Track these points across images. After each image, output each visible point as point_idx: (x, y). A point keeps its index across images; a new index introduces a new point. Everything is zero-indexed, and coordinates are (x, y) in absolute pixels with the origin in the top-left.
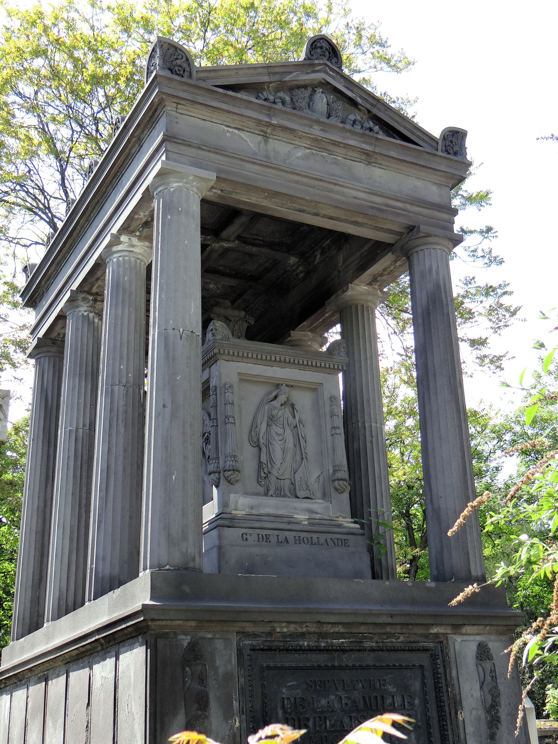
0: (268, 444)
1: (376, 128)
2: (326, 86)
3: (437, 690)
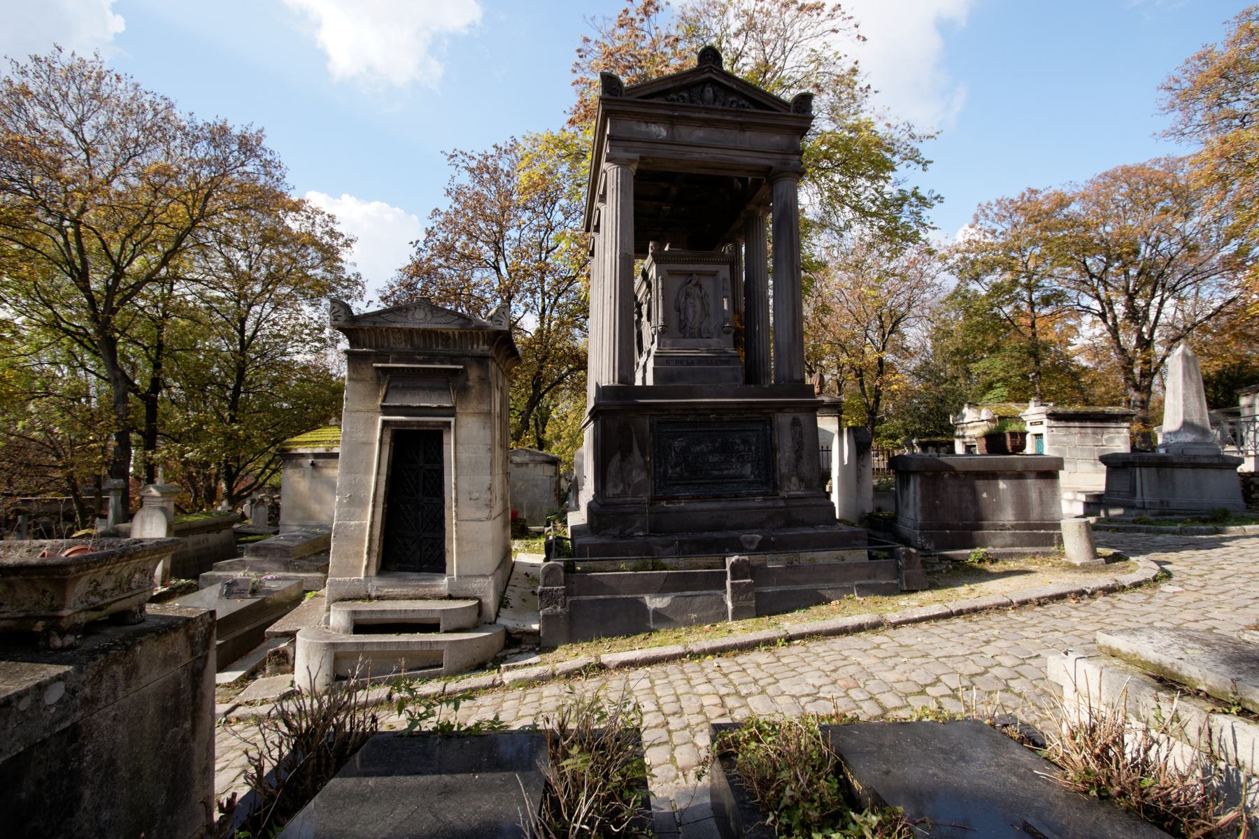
0: (686, 309)
1: (747, 104)
2: (711, 82)
3: (129, 643)
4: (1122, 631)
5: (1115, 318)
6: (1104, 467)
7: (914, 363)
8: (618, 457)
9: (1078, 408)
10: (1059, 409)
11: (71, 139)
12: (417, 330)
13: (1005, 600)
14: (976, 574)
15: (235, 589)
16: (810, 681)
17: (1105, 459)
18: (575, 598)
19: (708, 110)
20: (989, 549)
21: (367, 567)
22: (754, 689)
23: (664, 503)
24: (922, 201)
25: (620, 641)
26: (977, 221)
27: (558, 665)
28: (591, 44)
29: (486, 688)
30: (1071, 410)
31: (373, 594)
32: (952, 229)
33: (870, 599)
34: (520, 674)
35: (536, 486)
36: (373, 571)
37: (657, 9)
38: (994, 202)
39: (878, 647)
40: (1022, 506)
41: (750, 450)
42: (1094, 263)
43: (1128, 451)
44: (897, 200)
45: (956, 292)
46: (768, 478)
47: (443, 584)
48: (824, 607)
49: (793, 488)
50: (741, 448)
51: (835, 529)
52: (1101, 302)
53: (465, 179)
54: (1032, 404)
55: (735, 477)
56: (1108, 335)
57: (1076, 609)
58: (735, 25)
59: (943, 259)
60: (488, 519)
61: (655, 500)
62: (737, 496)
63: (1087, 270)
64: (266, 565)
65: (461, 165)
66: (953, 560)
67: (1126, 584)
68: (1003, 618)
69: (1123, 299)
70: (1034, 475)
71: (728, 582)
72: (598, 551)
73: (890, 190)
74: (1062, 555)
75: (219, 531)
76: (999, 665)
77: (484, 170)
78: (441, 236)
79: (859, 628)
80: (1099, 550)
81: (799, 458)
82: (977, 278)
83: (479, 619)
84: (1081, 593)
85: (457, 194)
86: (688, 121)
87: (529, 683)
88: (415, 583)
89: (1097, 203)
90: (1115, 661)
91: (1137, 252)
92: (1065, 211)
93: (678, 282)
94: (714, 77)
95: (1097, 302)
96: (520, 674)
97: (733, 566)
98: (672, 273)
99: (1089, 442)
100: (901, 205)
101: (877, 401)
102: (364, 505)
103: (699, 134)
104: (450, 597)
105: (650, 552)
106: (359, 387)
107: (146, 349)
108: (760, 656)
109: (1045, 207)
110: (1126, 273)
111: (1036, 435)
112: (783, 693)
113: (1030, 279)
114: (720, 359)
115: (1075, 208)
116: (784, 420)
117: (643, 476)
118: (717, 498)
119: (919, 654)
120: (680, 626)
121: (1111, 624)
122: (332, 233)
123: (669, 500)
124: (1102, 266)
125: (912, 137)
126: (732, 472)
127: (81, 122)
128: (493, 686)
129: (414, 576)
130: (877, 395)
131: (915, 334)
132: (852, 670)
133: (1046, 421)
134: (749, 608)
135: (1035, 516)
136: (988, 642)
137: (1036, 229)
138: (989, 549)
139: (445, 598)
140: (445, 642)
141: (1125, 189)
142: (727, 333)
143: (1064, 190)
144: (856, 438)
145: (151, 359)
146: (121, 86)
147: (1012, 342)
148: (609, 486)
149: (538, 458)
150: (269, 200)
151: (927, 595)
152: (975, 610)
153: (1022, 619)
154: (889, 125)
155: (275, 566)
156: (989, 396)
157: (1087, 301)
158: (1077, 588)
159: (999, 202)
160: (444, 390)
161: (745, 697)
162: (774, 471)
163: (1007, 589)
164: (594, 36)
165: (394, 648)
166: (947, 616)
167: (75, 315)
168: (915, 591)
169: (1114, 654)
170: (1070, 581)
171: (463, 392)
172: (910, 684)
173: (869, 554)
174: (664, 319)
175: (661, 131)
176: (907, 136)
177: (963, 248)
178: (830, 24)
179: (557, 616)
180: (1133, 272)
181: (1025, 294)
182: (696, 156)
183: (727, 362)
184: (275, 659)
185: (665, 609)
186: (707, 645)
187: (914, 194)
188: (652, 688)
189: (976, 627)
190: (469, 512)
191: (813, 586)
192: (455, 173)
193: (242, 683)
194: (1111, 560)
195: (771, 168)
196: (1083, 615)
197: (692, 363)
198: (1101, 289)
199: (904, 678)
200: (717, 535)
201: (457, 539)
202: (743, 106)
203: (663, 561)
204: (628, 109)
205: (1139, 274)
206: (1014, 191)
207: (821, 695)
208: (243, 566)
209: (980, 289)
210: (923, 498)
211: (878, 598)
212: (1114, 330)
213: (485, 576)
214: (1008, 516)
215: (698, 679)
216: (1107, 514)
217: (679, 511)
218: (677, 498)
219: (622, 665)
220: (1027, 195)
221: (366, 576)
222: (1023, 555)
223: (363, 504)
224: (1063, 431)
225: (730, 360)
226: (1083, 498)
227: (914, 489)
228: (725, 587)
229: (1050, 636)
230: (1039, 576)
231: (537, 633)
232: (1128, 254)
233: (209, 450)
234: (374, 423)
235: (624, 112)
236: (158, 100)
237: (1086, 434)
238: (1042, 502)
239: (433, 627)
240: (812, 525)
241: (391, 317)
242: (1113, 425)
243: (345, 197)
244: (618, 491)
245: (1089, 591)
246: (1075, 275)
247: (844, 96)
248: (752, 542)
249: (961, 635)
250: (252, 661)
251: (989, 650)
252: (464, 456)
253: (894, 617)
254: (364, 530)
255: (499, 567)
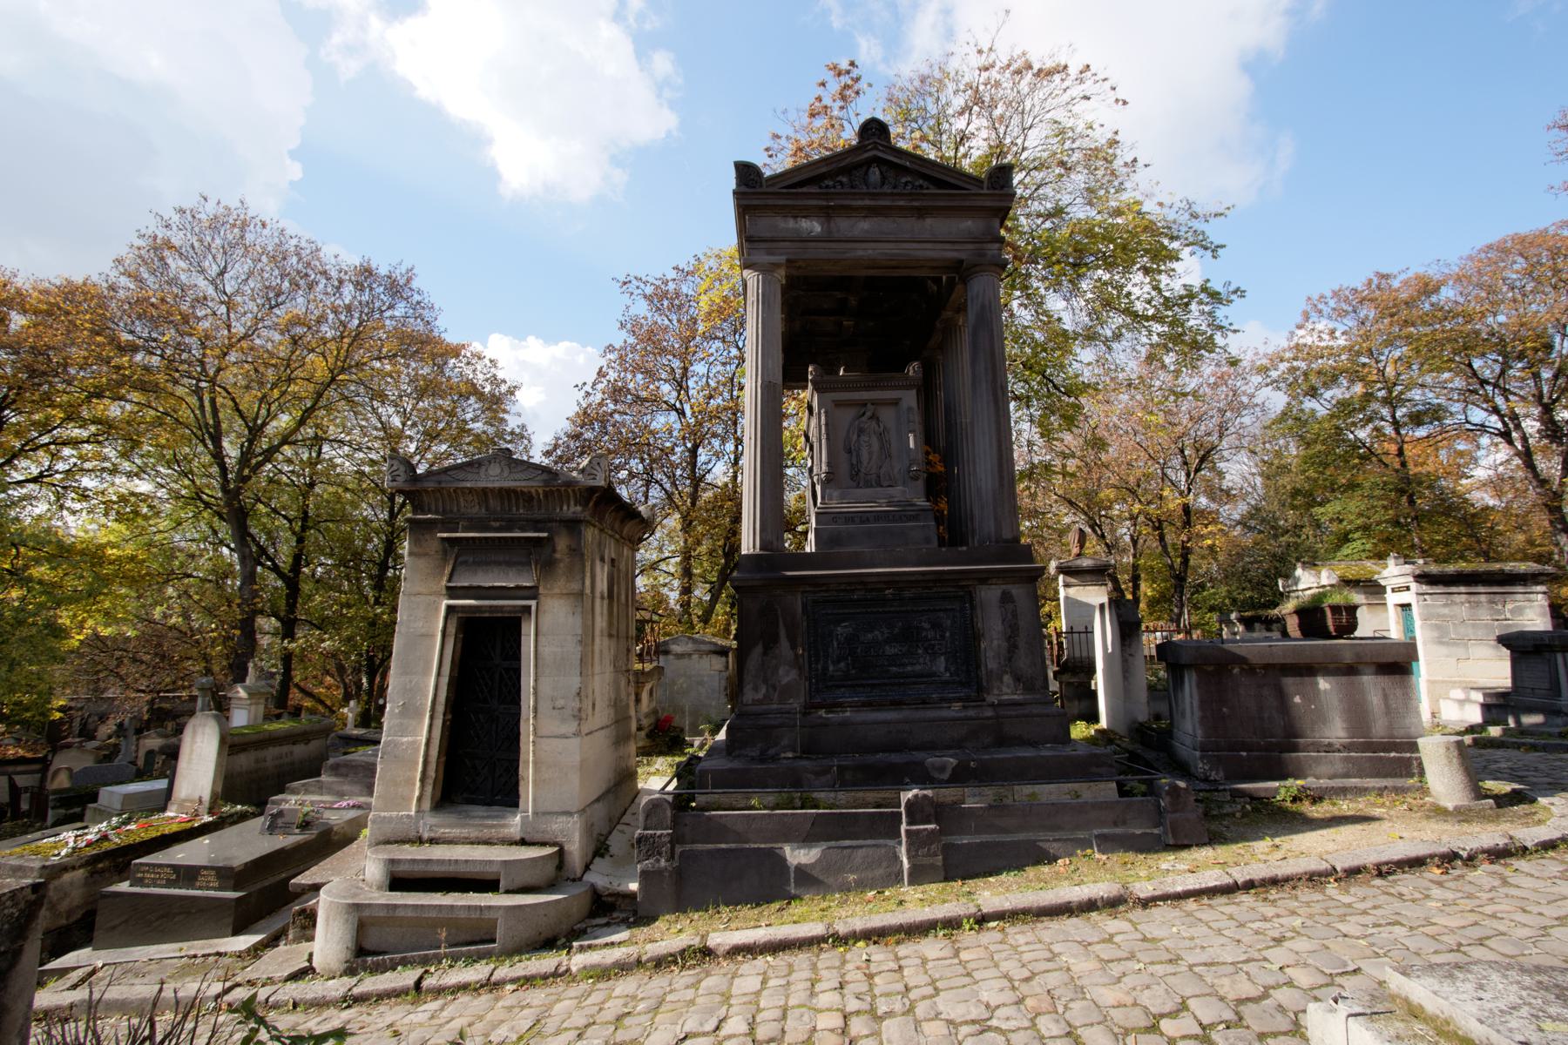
1: (925, 184)
4: (1432, 967)
5: (1524, 439)
6: (1506, 652)
7: (1238, 510)
8: (759, 649)
9: (1481, 566)
10: (1434, 569)
11: (211, 291)
12: (492, 490)
13: (1324, 866)
14: (1287, 820)
15: (280, 821)
16: (985, 996)
17: (1505, 640)
18: (688, 847)
19: (873, 196)
20: (1310, 781)
21: (420, 799)
22: (898, 1007)
23: (822, 713)
24: (1215, 296)
25: (746, 912)
26: (1307, 318)
27: (649, 947)
28: (783, 142)
29: (545, 977)
30: (1451, 568)
31: (426, 836)
32: (1257, 334)
33: (1117, 858)
34: (593, 958)
35: (701, 683)
36: (427, 805)
37: (857, 93)
38: (1329, 294)
39: (1110, 939)
40: (1357, 716)
41: (943, 637)
42: (1486, 366)
43: (1550, 628)
44: (1181, 298)
45: (1284, 415)
46: (969, 676)
47: (514, 824)
48: (1046, 869)
49: (1007, 691)
50: (931, 634)
51: (1068, 751)
52: (1501, 417)
53: (641, 308)
54: (1391, 562)
55: (922, 676)
56: (1517, 461)
57: (1440, 884)
58: (959, 102)
59: (1263, 370)
60: (577, 734)
61: (810, 708)
62: (924, 703)
63: (1475, 374)
64: (346, 788)
65: (636, 292)
66: (1253, 797)
67: (1529, 844)
68: (1317, 896)
69: (1536, 411)
70: (1373, 669)
71: (904, 827)
72: (727, 780)
73: (1173, 285)
74: (1424, 790)
75: (307, 742)
76: (1290, 983)
77: (661, 297)
78: (612, 375)
79: (1090, 906)
80: (1490, 784)
81: (1013, 648)
82: (1313, 393)
83: (557, 873)
84: (1449, 858)
85: (634, 326)
86: (848, 211)
87: (603, 973)
88: (481, 821)
89: (1480, 286)
90: (1418, 1027)
91: (1549, 347)
92: (1434, 299)
93: (848, 415)
94: (881, 155)
95: (1494, 418)
96: (593, 958)
97: (909, 804)
98: (838, 404)
99: (1484, 615)
100: (1187, 305)
101: (1186, 562)
102: (420, 715)
103: (864, 226)
104: (523, 842)
105: (797, 783)
106: (422, 563)
107: (290, 521)
108: (932, 947)
109: (1404, 296)
110: (1536, 376)
111: (1402, 606)
112: (937, 1016)
113: (1390, 392)
114: (906, 513)
115: (1447, 294)
116: (989, 594)
117: (793, 674)
118: (897, 704)
119: (1167, 956)
120: (833, 892)
121: (1494, 916)
122: (494, 381)
123: (830, 707)
124: (1497, 369)
125: (1195, 216)
126: (918, 668)
127: (222, 273)
128: (556, 974)
129: (480, 811)
130: (1186, 553)
131: (1237, 470)
132: (1053, 980)
133: (1414, 586)
134: (932, 866)
135: (1379, 730)
136: (1279, 941)
137: (1391, 324)
138: (1310, 781)
139: (516, 843)
140: (500, 908)
141: (1521, 263)
142: (916, 479)
143: (1431, 272)
144: (1119, 616)
145: (294, 533)
146: (266, 232)
147: (1372, 475)
148: (748, 689)
149: (703, 647)
150: (423, 345)
151: (1204, 854)
152: (1274, 882)
153: (1346, 899)
154: (1161, 204)
155: (356, 788)
156: (1346, 550)
157: (1478, 415)
158: (1444, 849)
159: (1335, 294)
160: (524, 564)
161: (881, 1019)
162: (978, 667)
163: (1331, 847)
164: (785, 130)
165: (433, 914)
166: (1229, 890)
167: (214, 490)
168: (1187, 847)
169: (1415, 1012)
170: (1434, 837)
171: (548, 567)
172: (1138, 1011)
173: (1120, 785)
174: (829, 464)
175: (814, 227)
176: (1187, 216)
177: (1288, 355)
178: (1076, 91)
179: (660, 872)
180: (1546, 374)
181: (1385, 412)
182: (860, 253)
183: (915, 518)
184: (300, 920)
185: (812, 865)
186: (858, 924)
187: (1204, 289)
188: (758, 993)
189: (1269, 911)
190: (551, 725)
191: (1031, 836)
192: (629, 302)
193: (255, 952)
194: (1503, 801)
195: (961, 262)
196: (1450, 895)
197: (868, 521)
198: (1499, 401)
199: (1129, 1001)
200: (895, 758)
201: (535, 763)
202: (921, 187)
203: (815, 795)
204: (770, 202)
205: (1556, 377)
206: (1356, 279)
207: (994, 1022)
208: (321, 789)
209: (1319, 407)
210: (1202, 702)
211: (1130, 856)
212: (1527, 456)
213: (569, 813)
214: (1336, 731)
215: (829, 980)
216: (1518, 722)
217: (845, 724)
218: (841, 705)
219: (736, 951)
220: (1376, 281)
221: (418, 812)
222: (1362, 791)
223: (418, 714)
224: (1442, 600)
225: (917, 515)
226: (1479, 697)
227: (1190, 692)
228: (899, 835)
229: (1385, 934)
230: (1386, 825)
231: (632, 895)
232: (1536, 350)
233: (350, 639)
234: (437, 610)
235: (766, 207)
236: (303, 244)
237: (1478, 603)
238: (1388, 710)
239: (488, 885)
240: (1033, 744)
241: (461, 475)
242: (1520, 589)
243: (531, 339)
244: (760, 696)
245: (1464, 854)
246: (1459, 383)
247: (1100, 173)
248: (942, 769)
249: (1241, 925)
250: (276, 923)
251: (1278, 956)
252: (546, 651)
253: (1144, 889)
254: (418, 750)
255: (598, 800)
